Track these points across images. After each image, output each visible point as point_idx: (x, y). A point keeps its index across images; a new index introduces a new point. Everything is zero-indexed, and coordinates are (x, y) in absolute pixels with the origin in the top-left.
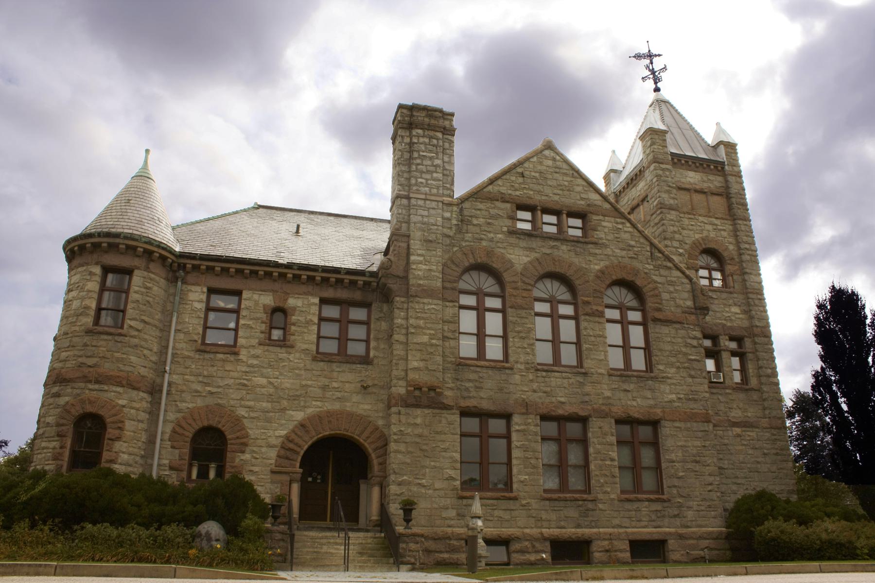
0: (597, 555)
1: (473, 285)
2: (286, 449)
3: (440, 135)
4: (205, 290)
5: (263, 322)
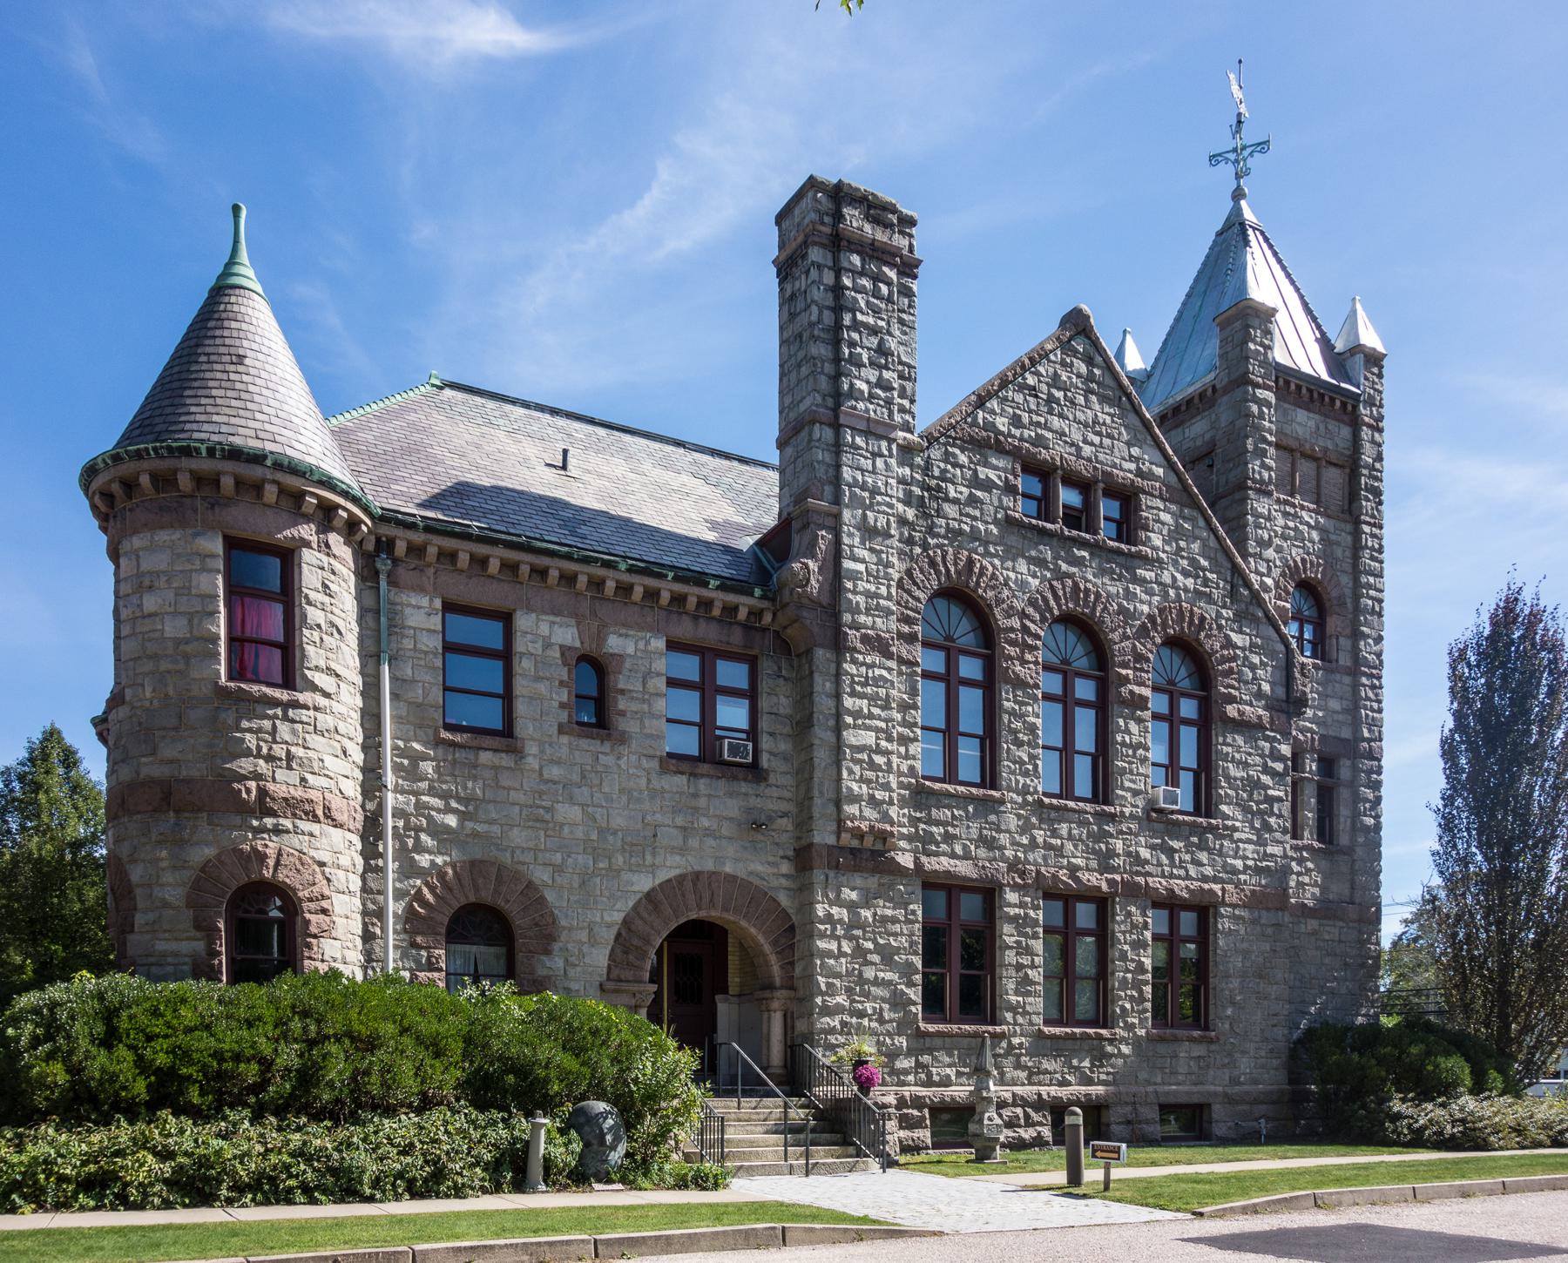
0: (1114, 1128)
1: (1062, 646)
2: (626, 941)
3: (892, 274)
4: (438, 603)
5: (622, 692)
